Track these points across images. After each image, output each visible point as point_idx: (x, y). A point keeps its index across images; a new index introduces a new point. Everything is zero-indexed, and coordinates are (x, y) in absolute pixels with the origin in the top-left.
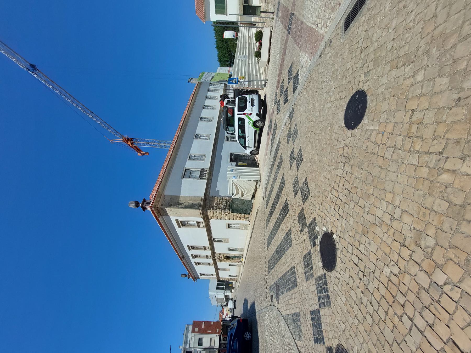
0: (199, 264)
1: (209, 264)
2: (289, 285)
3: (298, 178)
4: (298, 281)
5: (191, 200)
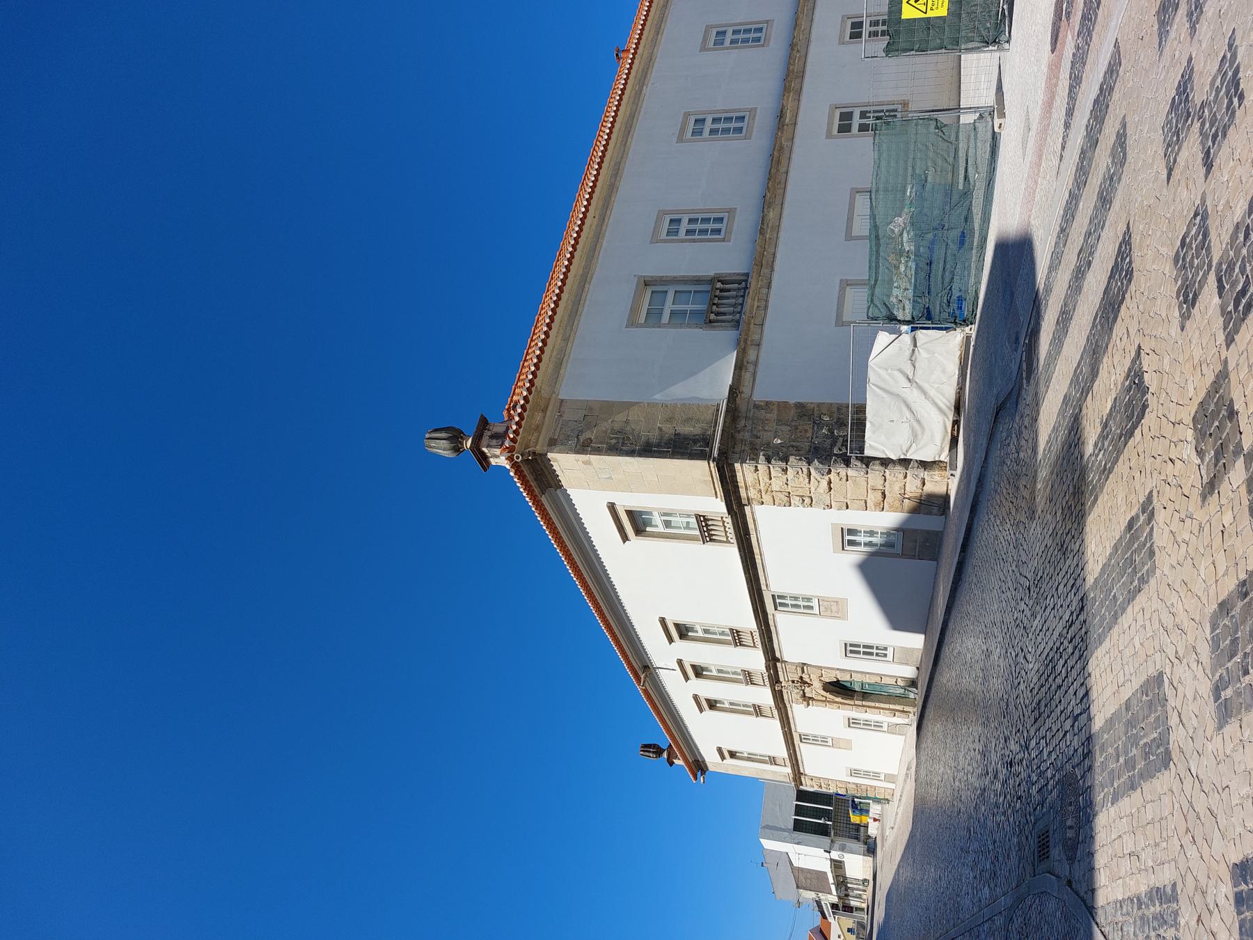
0: (712, 704)
1: (758, 711)
2: (1130, 764)
3: (1205, 217)
4: (1178, 737)
5: (670, 420)
